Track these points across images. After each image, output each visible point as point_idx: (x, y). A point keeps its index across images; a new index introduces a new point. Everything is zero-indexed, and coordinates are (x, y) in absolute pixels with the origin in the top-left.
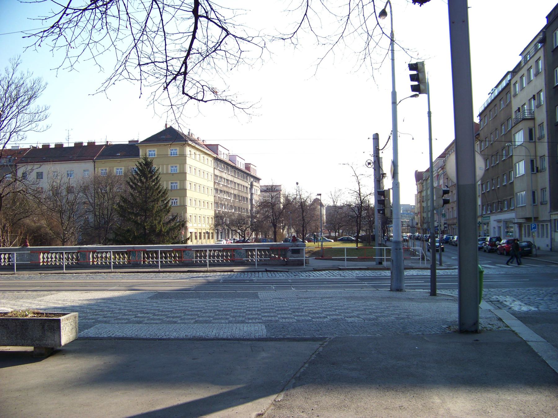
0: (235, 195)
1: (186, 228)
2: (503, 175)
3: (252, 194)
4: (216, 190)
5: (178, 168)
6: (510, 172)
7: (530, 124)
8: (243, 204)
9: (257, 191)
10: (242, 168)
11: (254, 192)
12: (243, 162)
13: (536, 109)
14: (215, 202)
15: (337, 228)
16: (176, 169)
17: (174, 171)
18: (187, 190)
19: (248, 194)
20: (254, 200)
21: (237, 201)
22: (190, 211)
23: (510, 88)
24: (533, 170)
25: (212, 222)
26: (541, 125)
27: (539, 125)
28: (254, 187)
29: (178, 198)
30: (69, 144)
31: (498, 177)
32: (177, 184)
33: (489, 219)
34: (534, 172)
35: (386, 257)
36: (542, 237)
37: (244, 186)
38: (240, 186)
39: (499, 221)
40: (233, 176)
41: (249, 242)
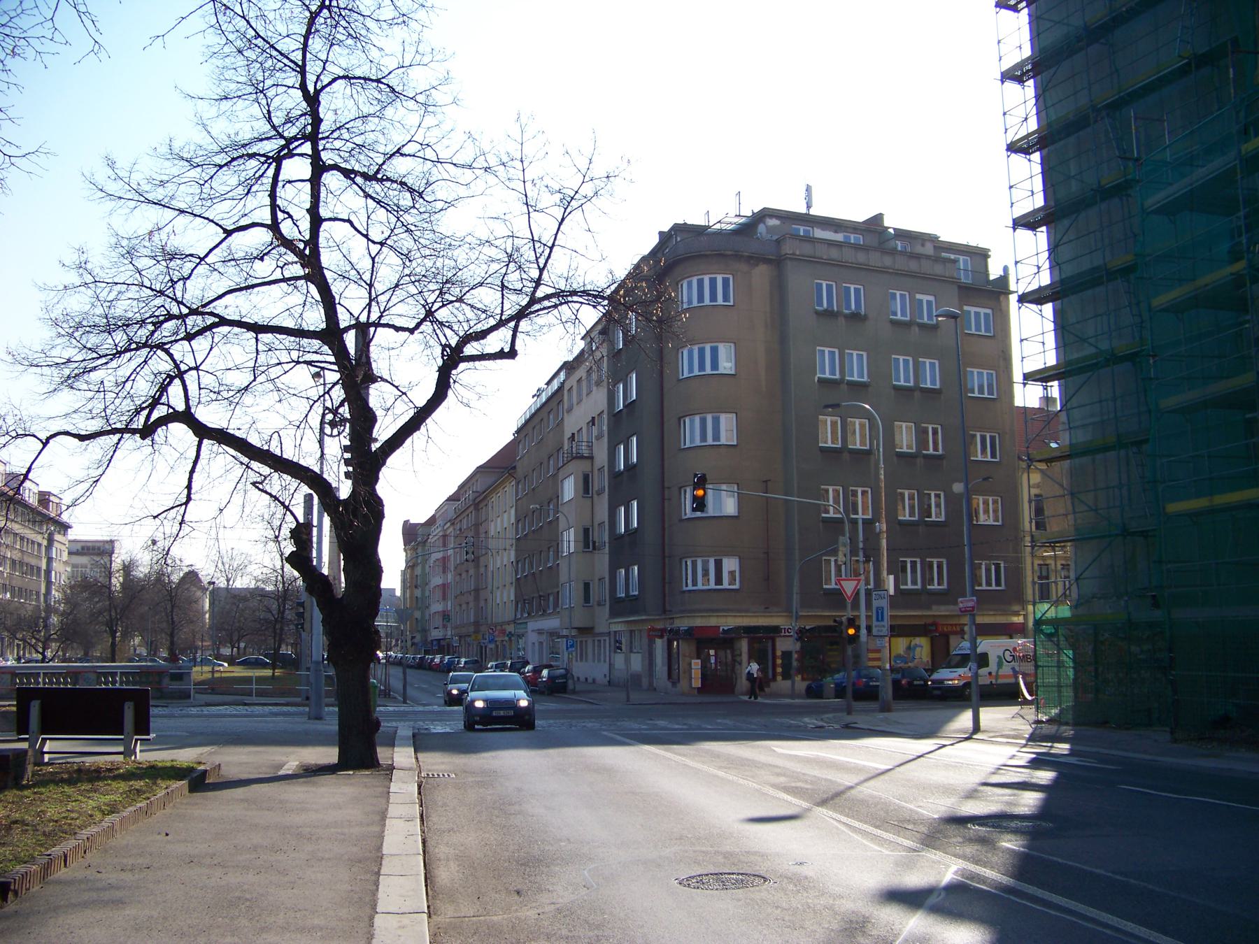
0: (13, 562)
3: (50, 560)
8: (29, 581)
9: (61, 551)
10: (31, 501)
11: (54, 556)
15: (235, 638)
19: (41, 560)
20: (53, 573)
21: (17, 574)
23: (563, 395)
24: (586, 545)
27: (599, 470)
28: (56, 544)
33: (526, 628)
36: (581, 660)
37: (33, 542)
39: (540, 632)
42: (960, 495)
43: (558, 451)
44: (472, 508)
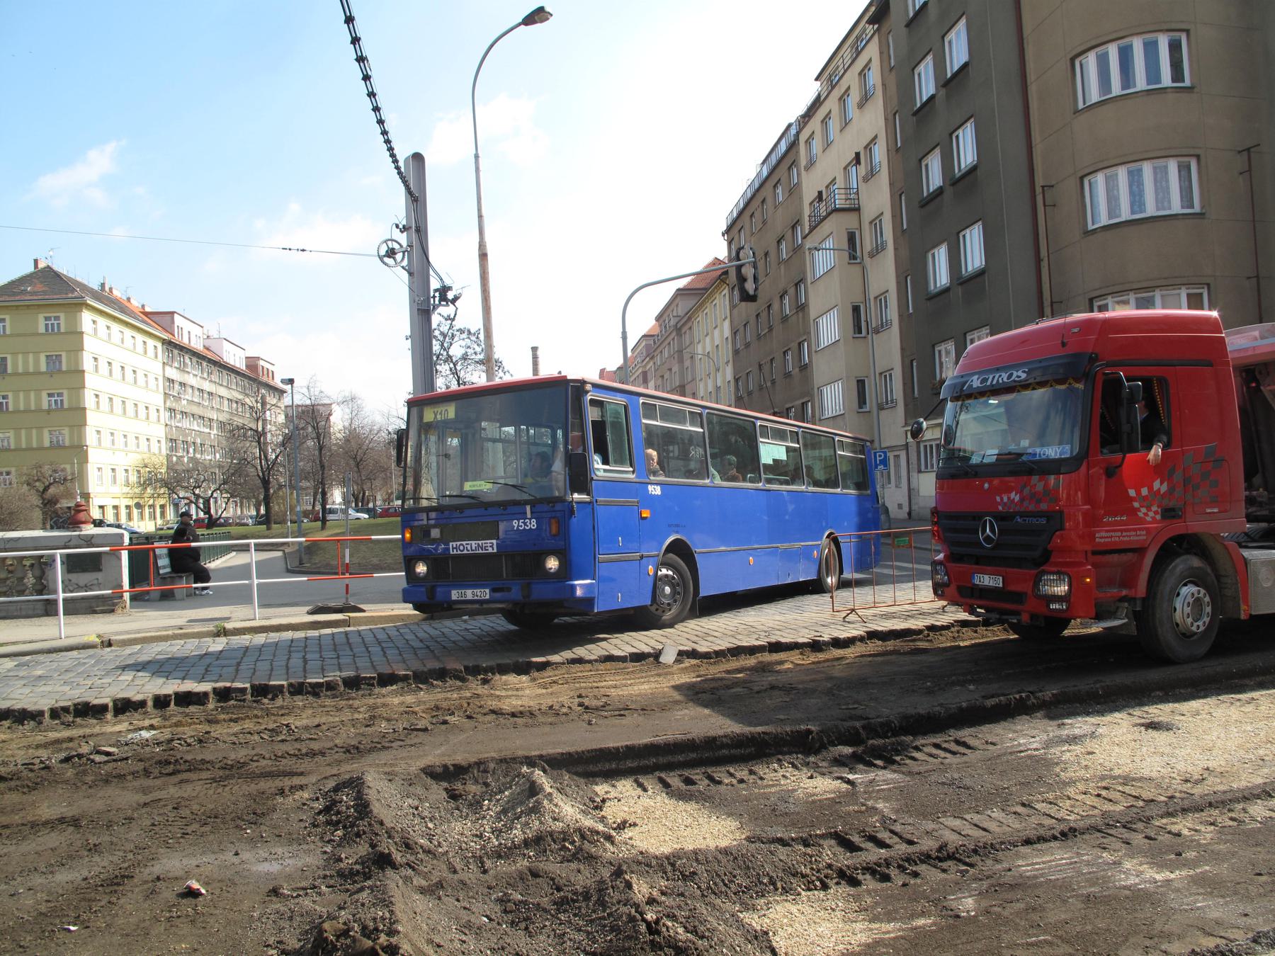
2: (784, 353)
6: (799, 344)
7: (849, 221)
12: (243, 354)
13: (863, 187)
18: (88, 411)
23: (798, 152)
26: (877, 221)
31: (772, 360)
32: (62, 396)
34: (860, 332)
35: (65, 600)
40: (215, 382)
43: (794, 227)
44: (674, 334)
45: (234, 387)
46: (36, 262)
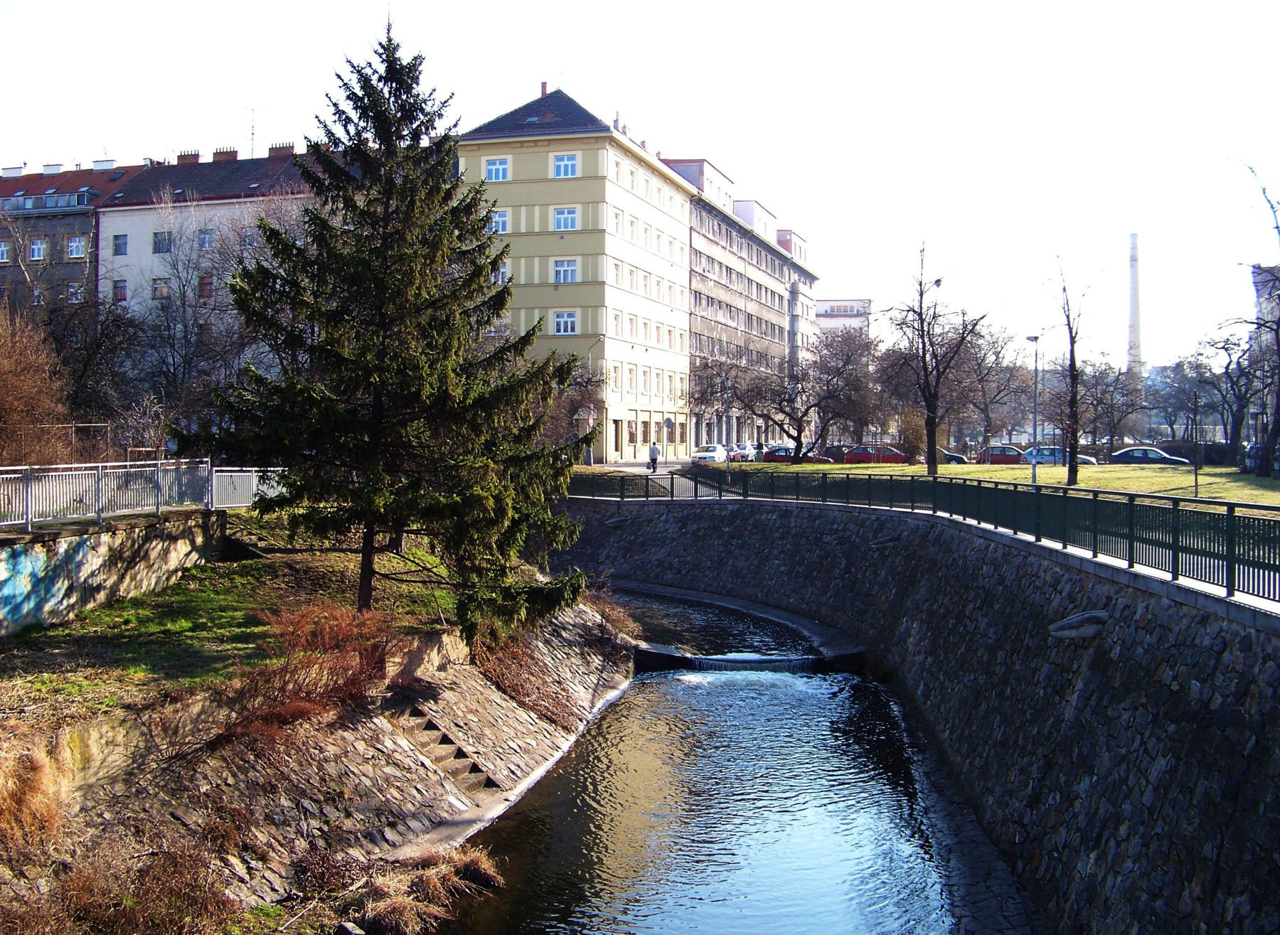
0: (750, 316)
1: (600, 406)
3: (794, 318)
4: (697, 295)
5: (578, 216)
14: (693, 330)
16: (573, 220)
17: (566, 226)
18: (607, 287)
21: (755, 333)
22: (615, 354)
25: (682, 385)
28: (801, 298)
29: (578, 312)
30: (253, 148)
38: (764, 290)
41: (810, 460)
42: (78, 263)
45: (763, 268)
46: (544, 85)
